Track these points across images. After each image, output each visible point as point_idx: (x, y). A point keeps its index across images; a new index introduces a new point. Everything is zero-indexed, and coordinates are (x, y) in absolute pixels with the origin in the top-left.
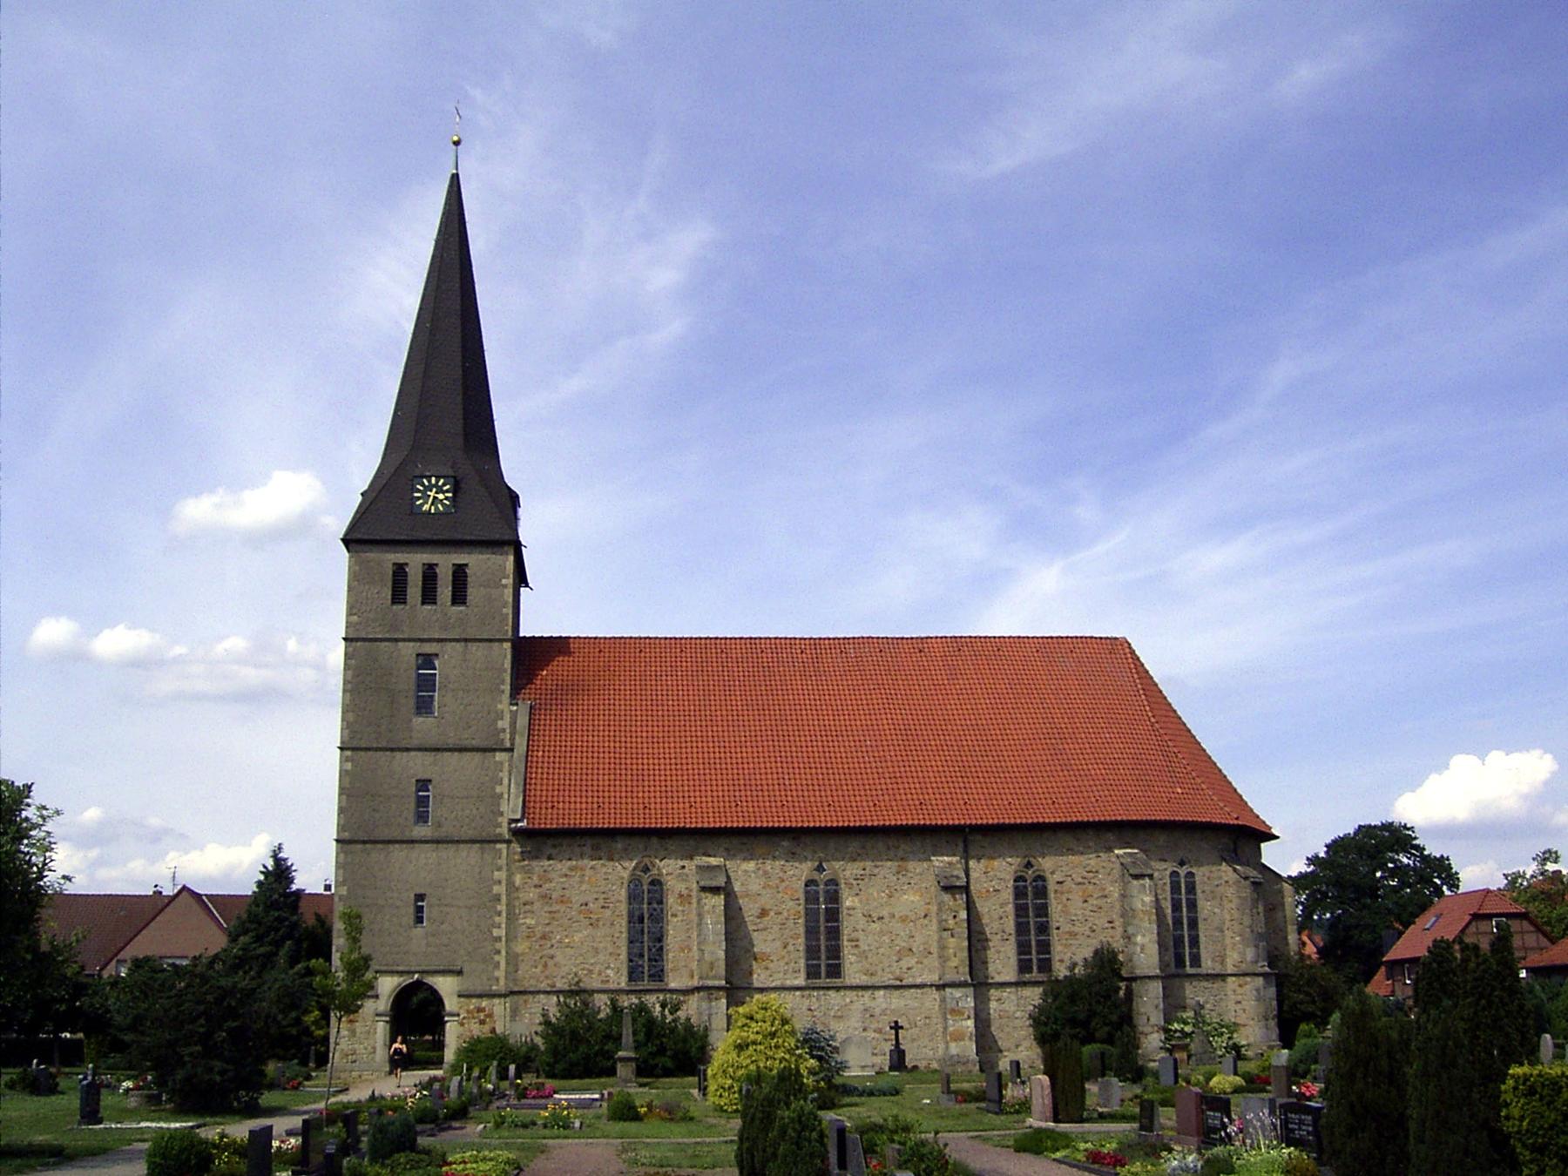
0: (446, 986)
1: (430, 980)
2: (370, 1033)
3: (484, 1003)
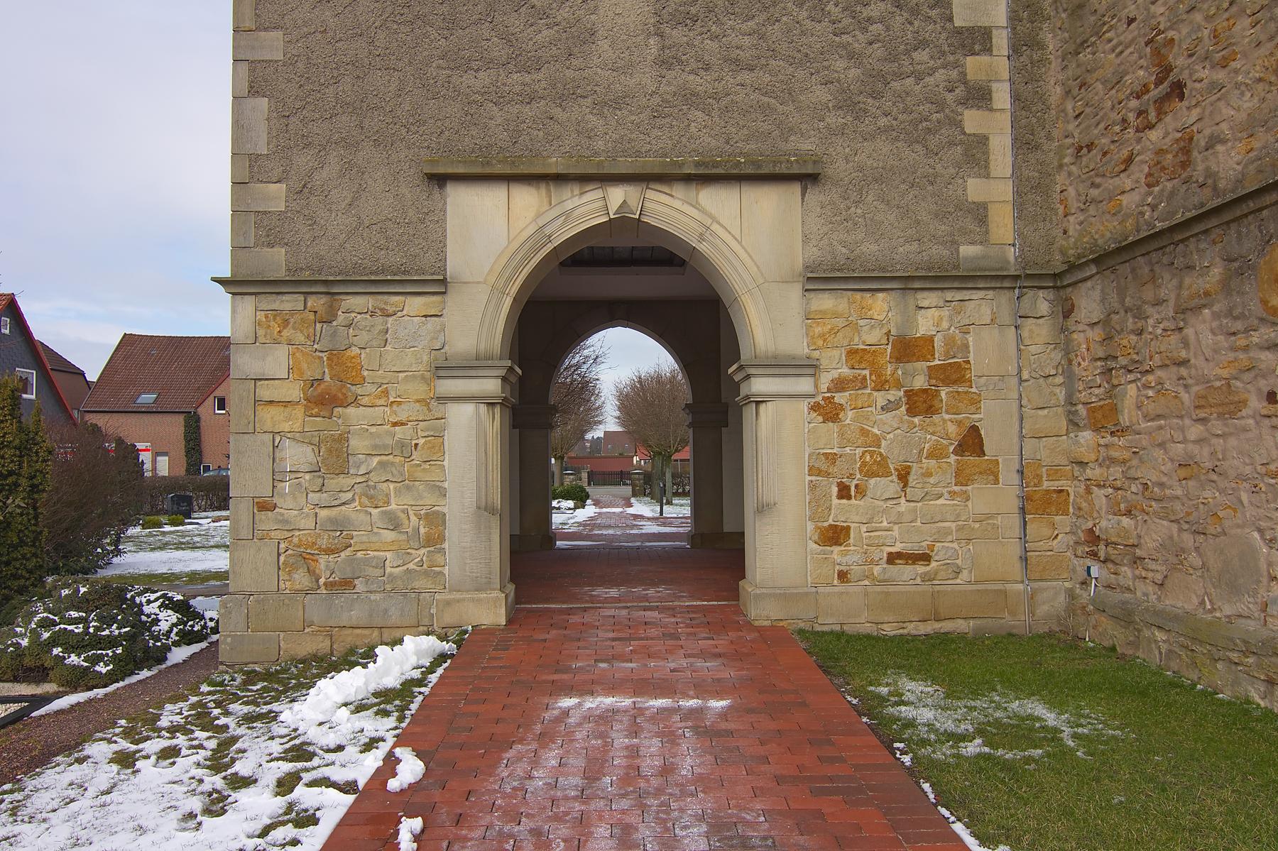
0: (746, 238)
1: (672, 211)
2: (417, 453)
3: (930, 317)
